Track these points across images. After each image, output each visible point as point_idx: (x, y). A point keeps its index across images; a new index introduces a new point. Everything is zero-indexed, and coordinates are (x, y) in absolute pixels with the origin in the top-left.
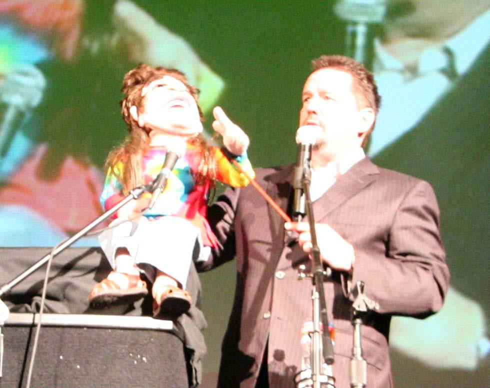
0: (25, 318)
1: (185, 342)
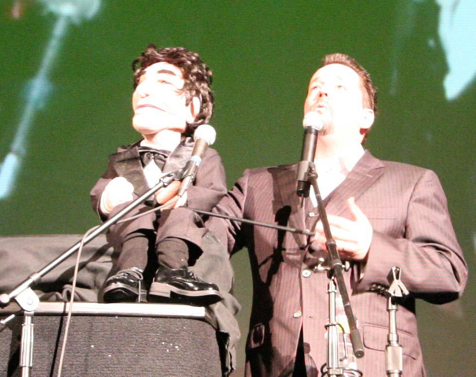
0: (56, 307)
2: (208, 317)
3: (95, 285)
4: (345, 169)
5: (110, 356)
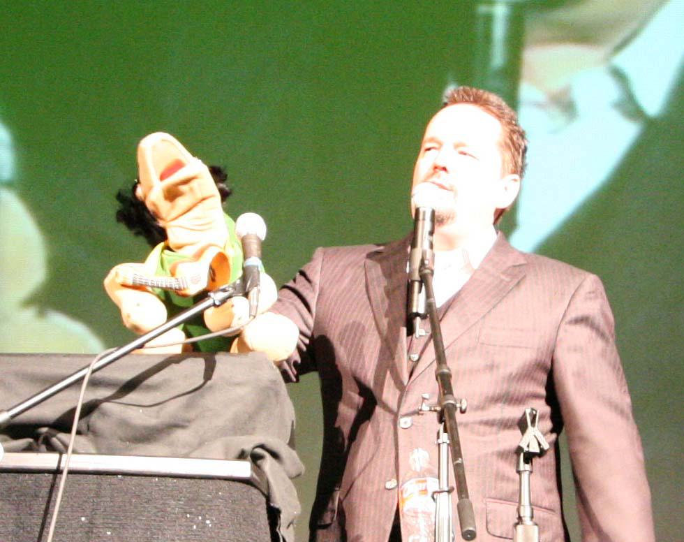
1: (268, 498)
2: (254, 479)
3: (88, 429)
4: (468, 265)
5: (109, 533)
